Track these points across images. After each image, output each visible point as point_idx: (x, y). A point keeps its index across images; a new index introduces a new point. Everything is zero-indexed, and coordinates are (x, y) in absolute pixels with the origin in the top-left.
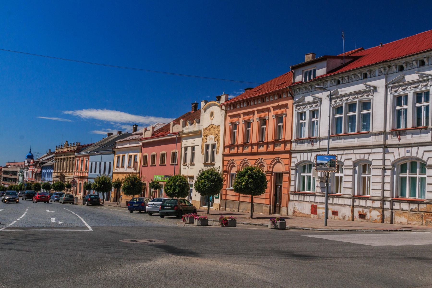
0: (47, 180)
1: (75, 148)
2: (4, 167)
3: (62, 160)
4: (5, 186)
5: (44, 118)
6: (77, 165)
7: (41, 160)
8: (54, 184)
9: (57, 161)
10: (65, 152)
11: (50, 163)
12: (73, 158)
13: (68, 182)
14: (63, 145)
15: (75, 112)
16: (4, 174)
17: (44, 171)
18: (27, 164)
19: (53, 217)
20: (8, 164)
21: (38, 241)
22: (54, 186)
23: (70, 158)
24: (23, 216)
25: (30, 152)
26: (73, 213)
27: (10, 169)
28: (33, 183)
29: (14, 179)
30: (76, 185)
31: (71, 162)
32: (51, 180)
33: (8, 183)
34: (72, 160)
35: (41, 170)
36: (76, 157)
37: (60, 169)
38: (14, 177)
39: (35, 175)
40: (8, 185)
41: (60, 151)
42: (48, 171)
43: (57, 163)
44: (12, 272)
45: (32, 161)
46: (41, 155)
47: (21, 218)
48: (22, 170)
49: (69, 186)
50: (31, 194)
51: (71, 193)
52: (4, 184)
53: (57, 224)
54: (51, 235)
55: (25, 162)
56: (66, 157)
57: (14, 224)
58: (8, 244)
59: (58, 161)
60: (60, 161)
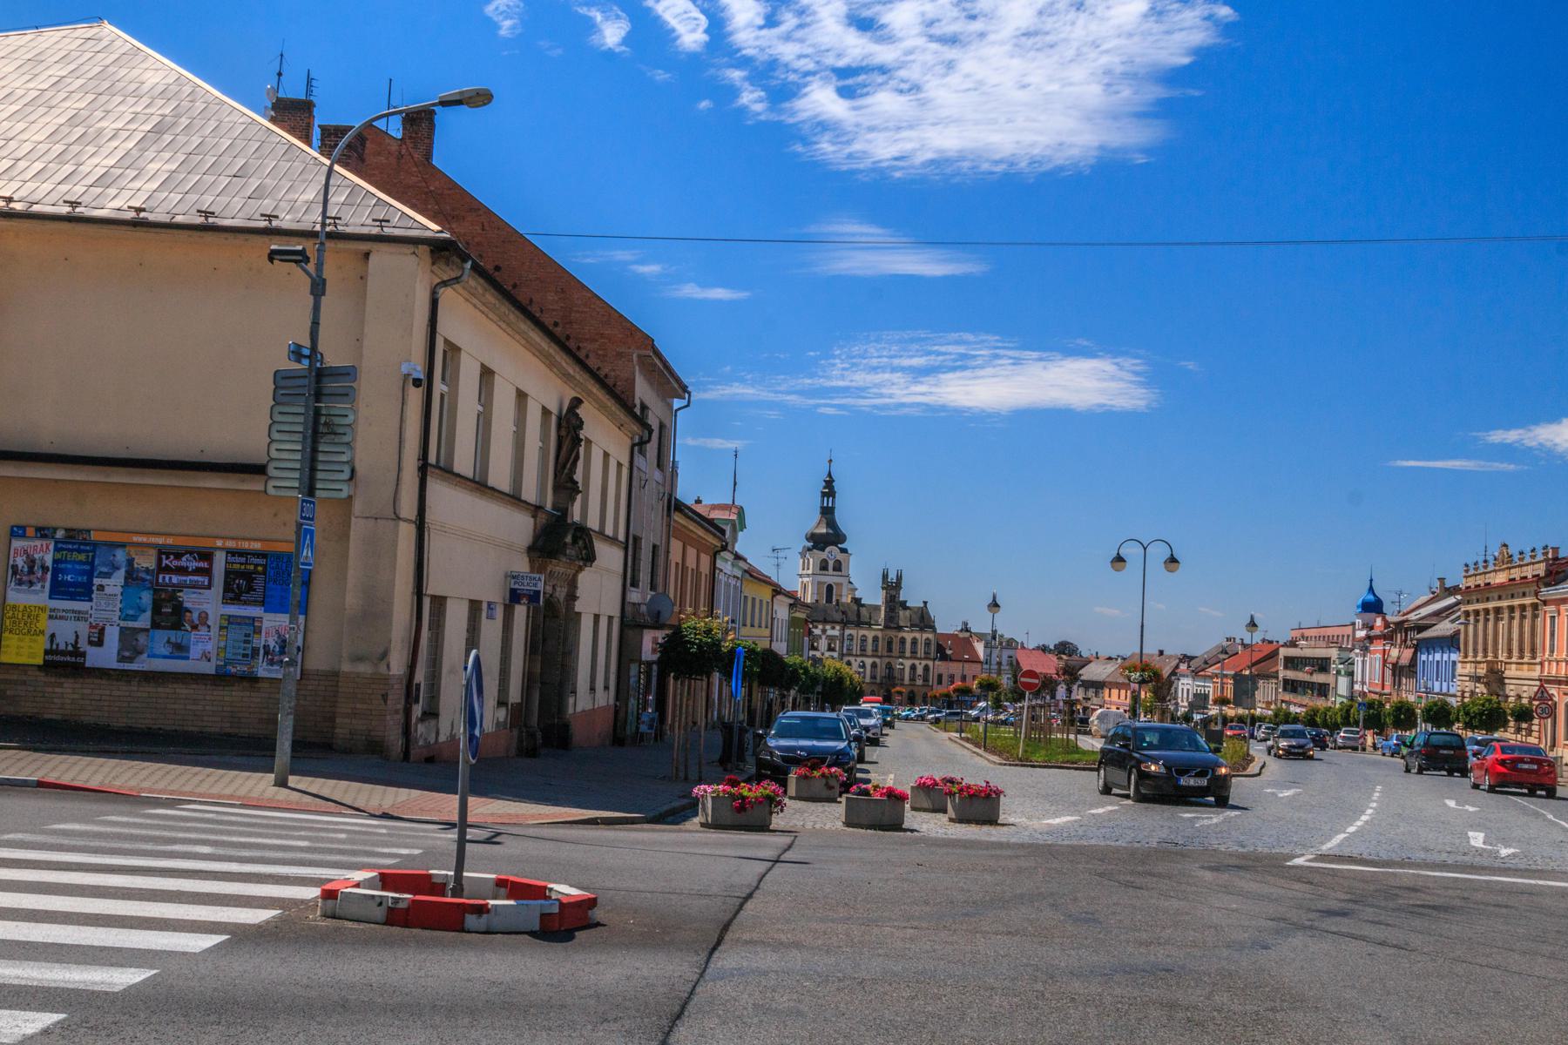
0: (1437, 689)
1: (1541, 569)
2: (1285, 645)
3: (1491, 617)
4: (1294, 709)
5: (1412, 463)
6: (1552, 634)
7: (1412, 617)
8: (1464, 706)
9: (1472, 619)
10: (1501, 586)
11: (1445, 628)
12: (1535, 607)
13: (1519, 697)
14: (1490, 559)
15: (1530, 434)
16: (1286, 667)
17: (1424, 657)
18: (1361, 634)
19: (1477, 827)
20: (1297, 634)
21: (1435, 913)
22: (1467, 714)
23: (1523, 608)
24: (1364, 818)
25: (1371, 589)
26: (1550, 817)
27: (1306, 650)
28: (1388, 701)
29: (1321, 685)
30: (1552, 712)
31: (1527, 623)
32: (1452, 691)
33: (1299, 699)
34: (1529, 613)
35: (1415, 654)
36: (1545, 603)
37: (1485, 650)
38: (1319, 678)
39: (1394, 670)
40: (1301, 706)
41: (1480, 581)
42: (1438, 656)
43: (1471, 628)
44: (1361, 1017)
45: (1379, 622)
46: (1410, 598)
47: (1359, 823)
48: (1345, 655)
49: (1524, 715)
50: (1445, 747)
51: (1532, 740)
52: (1289, 703)
53: (1495, 855)
54: (1479, 896)
55: (1353, 624)
56: (1504, 604)
57: (1339, 845)
58: (1330, 913)
59: (1477, 621)
60: (1481, 618)
